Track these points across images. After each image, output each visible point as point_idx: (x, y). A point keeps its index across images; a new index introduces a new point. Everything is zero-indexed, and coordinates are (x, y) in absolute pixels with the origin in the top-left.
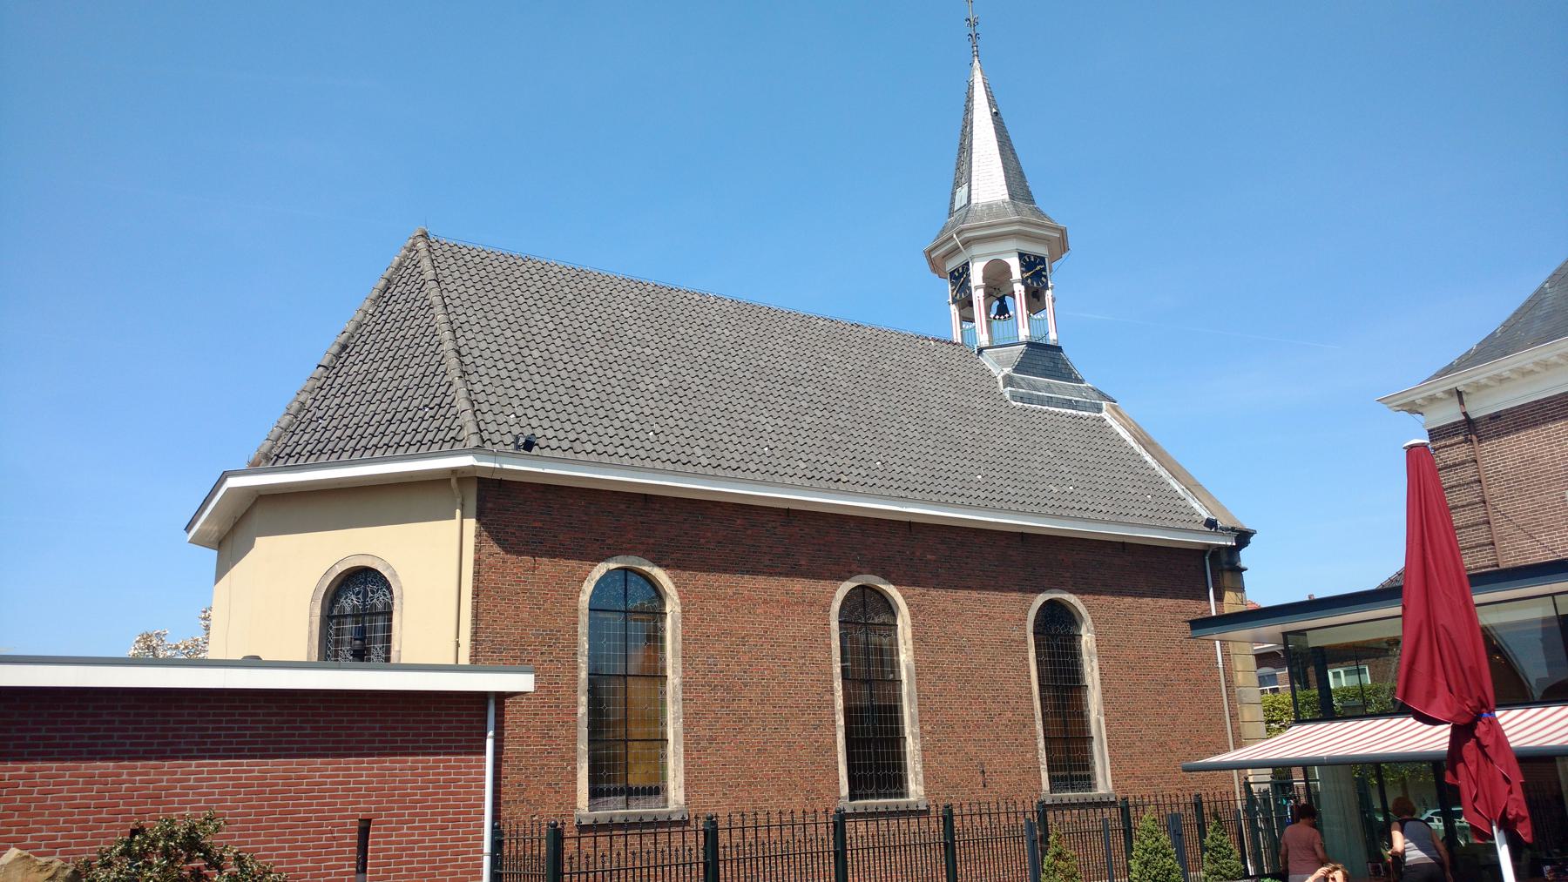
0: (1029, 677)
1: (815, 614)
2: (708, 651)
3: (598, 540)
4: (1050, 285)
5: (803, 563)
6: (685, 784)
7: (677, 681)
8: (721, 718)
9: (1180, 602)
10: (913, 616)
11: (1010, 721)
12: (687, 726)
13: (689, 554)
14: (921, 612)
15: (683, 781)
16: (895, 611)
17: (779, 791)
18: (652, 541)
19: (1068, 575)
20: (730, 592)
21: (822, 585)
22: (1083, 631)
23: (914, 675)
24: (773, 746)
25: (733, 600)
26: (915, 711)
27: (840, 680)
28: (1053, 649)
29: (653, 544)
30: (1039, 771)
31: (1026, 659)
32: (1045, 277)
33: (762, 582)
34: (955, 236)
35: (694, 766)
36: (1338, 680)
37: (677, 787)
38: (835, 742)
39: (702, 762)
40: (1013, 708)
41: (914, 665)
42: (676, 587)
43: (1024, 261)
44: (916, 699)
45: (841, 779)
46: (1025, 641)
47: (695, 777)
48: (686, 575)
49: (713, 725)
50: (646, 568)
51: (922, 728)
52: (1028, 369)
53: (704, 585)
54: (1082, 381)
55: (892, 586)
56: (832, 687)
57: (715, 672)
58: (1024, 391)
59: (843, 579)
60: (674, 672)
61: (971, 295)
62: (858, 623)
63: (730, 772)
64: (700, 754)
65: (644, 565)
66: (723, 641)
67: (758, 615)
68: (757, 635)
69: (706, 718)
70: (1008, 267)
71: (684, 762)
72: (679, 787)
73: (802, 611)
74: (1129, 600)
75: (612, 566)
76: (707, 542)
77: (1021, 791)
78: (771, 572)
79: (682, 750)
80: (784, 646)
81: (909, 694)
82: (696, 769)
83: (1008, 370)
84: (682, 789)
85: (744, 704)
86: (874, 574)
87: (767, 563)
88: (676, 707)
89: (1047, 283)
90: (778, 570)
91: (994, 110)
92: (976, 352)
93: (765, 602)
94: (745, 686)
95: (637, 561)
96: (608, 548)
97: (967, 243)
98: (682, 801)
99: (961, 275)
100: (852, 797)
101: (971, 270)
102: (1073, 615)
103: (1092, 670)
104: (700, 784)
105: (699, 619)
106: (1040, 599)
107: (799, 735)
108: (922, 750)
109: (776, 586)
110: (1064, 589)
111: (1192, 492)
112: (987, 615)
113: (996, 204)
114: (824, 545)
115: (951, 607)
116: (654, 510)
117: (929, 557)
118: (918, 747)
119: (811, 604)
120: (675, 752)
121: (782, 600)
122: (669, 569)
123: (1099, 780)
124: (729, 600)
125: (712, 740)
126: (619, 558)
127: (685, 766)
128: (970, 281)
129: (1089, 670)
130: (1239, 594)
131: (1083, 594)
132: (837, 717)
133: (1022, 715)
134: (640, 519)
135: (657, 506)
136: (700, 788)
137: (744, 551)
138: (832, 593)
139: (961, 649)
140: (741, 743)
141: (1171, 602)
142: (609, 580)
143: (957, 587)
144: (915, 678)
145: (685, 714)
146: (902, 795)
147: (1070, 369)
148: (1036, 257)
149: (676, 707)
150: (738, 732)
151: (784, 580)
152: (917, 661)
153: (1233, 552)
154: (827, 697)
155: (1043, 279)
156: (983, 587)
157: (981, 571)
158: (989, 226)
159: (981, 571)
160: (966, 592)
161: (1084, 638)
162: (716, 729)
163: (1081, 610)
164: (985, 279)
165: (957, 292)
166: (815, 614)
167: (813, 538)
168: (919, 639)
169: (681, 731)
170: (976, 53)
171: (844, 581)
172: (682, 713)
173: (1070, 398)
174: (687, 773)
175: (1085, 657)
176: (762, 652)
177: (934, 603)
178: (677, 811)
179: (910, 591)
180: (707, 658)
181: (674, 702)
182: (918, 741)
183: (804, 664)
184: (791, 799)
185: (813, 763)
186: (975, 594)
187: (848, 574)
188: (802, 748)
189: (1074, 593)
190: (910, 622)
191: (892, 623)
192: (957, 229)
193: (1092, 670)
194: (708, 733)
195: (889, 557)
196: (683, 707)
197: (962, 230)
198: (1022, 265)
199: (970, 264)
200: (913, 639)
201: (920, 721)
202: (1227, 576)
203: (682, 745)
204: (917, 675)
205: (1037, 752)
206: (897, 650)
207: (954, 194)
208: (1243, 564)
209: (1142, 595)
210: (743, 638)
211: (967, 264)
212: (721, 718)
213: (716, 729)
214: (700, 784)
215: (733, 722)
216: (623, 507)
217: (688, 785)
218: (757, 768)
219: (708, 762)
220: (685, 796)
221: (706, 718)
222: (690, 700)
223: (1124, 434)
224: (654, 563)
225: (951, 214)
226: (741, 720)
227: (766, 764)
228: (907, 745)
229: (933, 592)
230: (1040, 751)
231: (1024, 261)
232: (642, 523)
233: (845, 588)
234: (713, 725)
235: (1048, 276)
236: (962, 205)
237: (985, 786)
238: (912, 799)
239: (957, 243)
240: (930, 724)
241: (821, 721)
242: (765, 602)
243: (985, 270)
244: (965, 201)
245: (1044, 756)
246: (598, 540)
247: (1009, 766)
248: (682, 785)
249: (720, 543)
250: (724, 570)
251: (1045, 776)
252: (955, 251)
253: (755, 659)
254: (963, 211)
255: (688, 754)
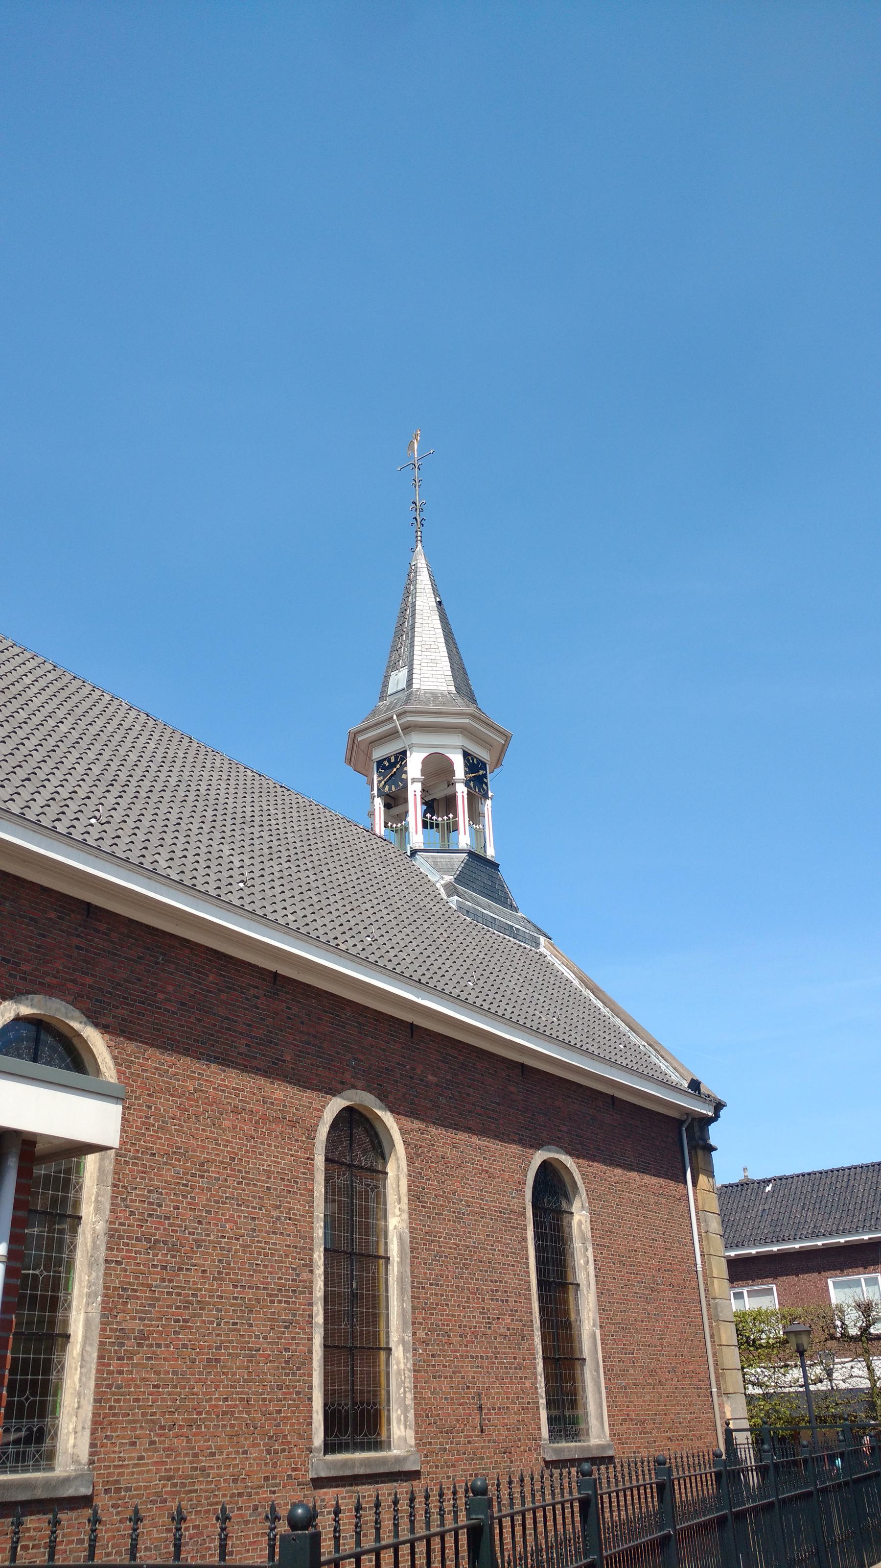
0: (527, 1264)
1: (297, 1141)
2: (151, 1179)
3: (8, 961)
4: (490, 794)
5: (288, 1058)
6: (94, 1423)
7: (101, 1227)
8: (158, 1299)
9: (662, 1181)
10: (410, 1160)
11: (508, 1329)
12: (108, 1311)
13: (138, 1013)
14: (419, 1155)
15: (90, 1415)
16: (386, 1151)
17: (231, 1437)
18: (89, 980)
19: (565, 1129)
20: (190, 1085)
21: (308, 1096)
22: (576, 1207)
23: (408, 1250)
24: (229, 1354)
25: (193, 1100)
26: (408, 1306)
27: (322, 1249)
28: (546, 1230)
29: (91, 986)
30: (538, 1408)
31: (525, 1239)
32: (486, 784)
33: (233, 1079)
34: (395, 717)
35: (109, 1386)
36: (741, 1301)
37: (79, 1428)
38: (310, 1352)
39: (123, 1380)
40: (512, 1311)
41: (409, 1235)
42: (117, 1064)
43: (468, 760)
44: (409, 1288)
45: (314, 1416)
46: (524, 1214)
47: (111, 1408)
48: (131, 1047)
49: (145, 1312)
50: (76, 1025)
51: (414, 1334)
52: (469, 883)
53: (156, 1068)
54: (516, 910)
55: (389, 1114)
56: (311, 1260)
57: (158, 1217)
58: (470, 904)
59: (334, 1092)
60: (97, 1210)
61: (405, 787)
62: (343, 1164)
63: (163, 1400)
64: (122, 1365)
65: (73, 1018)
66: (174, 1166)
67: (224, 1130)
68: (222, 1163)
69: (138, 1298)
70: (450, 764)
71: (97, 1379)
72: (84, 1428)
73: (281, 1133)
74: (618, 1171)
75: (25, 1010)
76: (166, 999)
77: (519, 1440)
78: (247, 1066)
79: (95, 1355)
80: (255, 1185)
81: (401, 1280)
82: (114, 1394)
83: (449, 878)
84: (87, 1433)
85: (195, 1277)
86: (370, 1092)
87: (243, 1049)
88: (94, 1274)
89: (488, 791)
90: (255, 1063)
91: (438, 599)
92: (409, 854)
93: (236, 1111)
94: (199, 1246)
95: (63, 1009)
96: (21, 978)
97: (408, 728)
98: (84, 1457)
99: (392, 765)
100: (329, 1447)
101: (408, 760)
102: (564, 1185)
103: (587, 1263)
104: (117, 1422)
105: (144, 1123)
106: (539, 1157)
107: (265, 1338)
108: (415, 1371)
109: (251, 1088)
110: (561, 1147)
111: (655, 1050)
112: (487, 1172)
113: (442, 694)
114: (315, 1037)
115: (451, 1154)
116: (96, 930)
117: (430, 1078)
118: (410, 1365)
119: (293, 1124)
120: (83, 1360)
121: (258, 1111)
122: (107, 1032)
123: (593, 1422)
124: (187, 1098)
125: (143, 1337)
126: (37, 998)
127: (97, 1386)
128: (406, 772)
129: (582, 1262)
130: (710, 1179)
131: (578, 1158)
132: (315, 1308)
133: (521, 1321)
134: (75, 941)
135: (103, 927)
136: (116, 1430)
137: (215, 1025)
138: (319, 1110)
139: (459, 1217)
140: (185, 1346)
141: (654, 1180)
142: (11, 1035)
143: (457, 1127)
144: (409, 1255)
145: (106, 1288)
146: (377, 1445)
147: (506, 893)
148: (479, 761)
149: (94, 1274)
150: (181, 1327)
151: (262, 1081)
152: (412, 1230)
153: (708, 1121)
154: (305, 1275)
155: (484, 785)
156: (483, 1132)
157: (482, 1107)
158: (436, 713)
159: (482, 1107)
160: (466, 1135)
161: (576, 1218)
162: (150, 1319)
163: (576, 1178)
164: (423, 772)
165: (385, 783)
166: (297, 1141)
167: (302, 1023)
168: (416, 1197)
169: (97, 1319)
170: (419, 538)
171: (334, 1095)
172: (101, 1286)
173: (512, 924)
174: (98, 1400)
175: (577, 1244)
176: (225, 1192)
177: (433, 1145)
178: (76, 1478)
179: (409, 1124)
180: (150, 1191)
181: (90, 1265)
182: (410, 1355)
183: (278, 1218)
184: (245, 1452)
185: (280, 1387)
186: (475, 1140)
187: (340, 1086)
188: (267, 1359)
189: (571, 1155)
190: (406, 1170)
191: (380, 1168)
192: (399, 709)
193: (587, 1263)
194: (137, 1325)
195: (387, 1069)
196: (106, 1274)
197: (405, 712)
198: (466, 765)
199: (408, 753)
200: (409, 1195)
201: (413, 1323)
202: (700, 1153)
203: (96, 1345)
204: (413, 1249)
205: (536, 1378)
206: (385, 1210)
207: (387, 677)
208: (713, 1141)
209: (631, 1169)
210: (202, 1165)
211: (404, 753)
212: (158, 1299)
213: (150, 1319)
214: (117, 1422)
215: (178, 1308)
216: (53, 915)
217: (98, 1424)
218: (204, 1394)
219: (133, 1380)
220: (92, 1445)
221: (138, 1298)
222: (117, 1263)
223: (570, 976)
224: (88, 1017)
225: (382, 698)
226: (187, 1304)
227: (217, 1387)
228: (393, 1361)
229: (432, 1130)
230: (539, 1377)
231: (468, 760)
232: (79, 948)
233: (335, 1105)
234: (145, 1312)
235: (489, 783)
236: (400, 688)
237: (482, 1431)
238: (395, 1452)
239: (396, 726)
240: (424, 1329)
241: (294, 1315)
242: (236, 1111)
243: (425, 762)
244: (403, 685)
245: (543, 1385)
246: (8, 961)
247: (508, 1398)
248: (88, 1424)
249: (183, 1004)
250: (185, 1049)
251: (544, 1414)
252: (392, 735)
253: (217, 1202)
254: (402, 696)
255: (103, 1365)
